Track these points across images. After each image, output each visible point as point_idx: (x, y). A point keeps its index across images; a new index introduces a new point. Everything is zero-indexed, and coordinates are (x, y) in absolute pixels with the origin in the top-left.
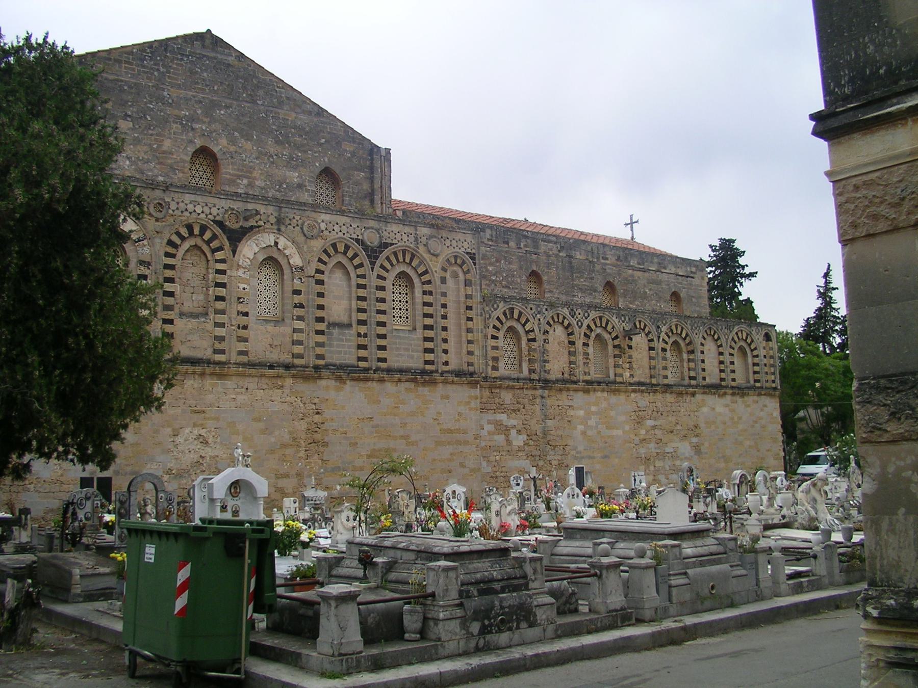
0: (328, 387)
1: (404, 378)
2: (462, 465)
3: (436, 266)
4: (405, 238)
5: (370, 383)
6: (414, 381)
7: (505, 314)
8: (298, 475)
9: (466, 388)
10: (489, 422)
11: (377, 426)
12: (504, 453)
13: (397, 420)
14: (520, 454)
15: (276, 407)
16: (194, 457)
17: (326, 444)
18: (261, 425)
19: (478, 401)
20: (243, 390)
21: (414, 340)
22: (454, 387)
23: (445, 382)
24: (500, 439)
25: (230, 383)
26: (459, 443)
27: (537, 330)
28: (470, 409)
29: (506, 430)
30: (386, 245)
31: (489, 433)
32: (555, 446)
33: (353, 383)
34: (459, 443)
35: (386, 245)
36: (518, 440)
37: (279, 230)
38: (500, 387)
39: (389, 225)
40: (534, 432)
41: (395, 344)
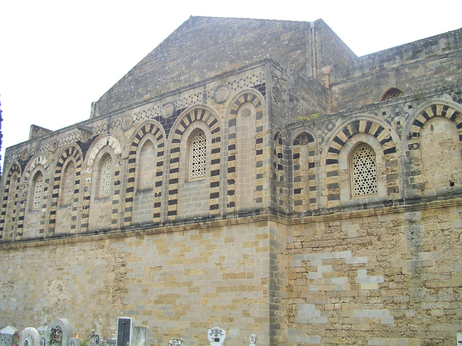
0: (131, 243)
1: (188, 226)
2: (246, 314)
3: (222, 114)
4: (195, 99)
5: (161, 236)
6: (197, 227)
7: (346, 131)
8: (107, 315)
9: (253, 227)
10: (325, 262)
11: (165, 274)
12: (347, 300)
13: (182, 268)
14: (374, 300)
15: (98, 262)
16: (54, 300)
17: (126, 291)
18: (89, 277)
19: (268, 240)
20: (83, 252)
21: (202, 188)
22: (239, 228)
23: (229, 224)
24: (341, 282)
25: (76, 248)
26: (243, 288)
27: (395, 137)
28: (258, 250)
29: (351, 271)
30: (179, 112)
31: (324, 275)
32: (437, 290)
33: (150, 237)
34: (243, 288)
35: (179, 112)
36: (369, 283)
37: (109, 133)
38: (340, 218)
39: (182, 94)
40: (398, 271)
41: (186, 196)
